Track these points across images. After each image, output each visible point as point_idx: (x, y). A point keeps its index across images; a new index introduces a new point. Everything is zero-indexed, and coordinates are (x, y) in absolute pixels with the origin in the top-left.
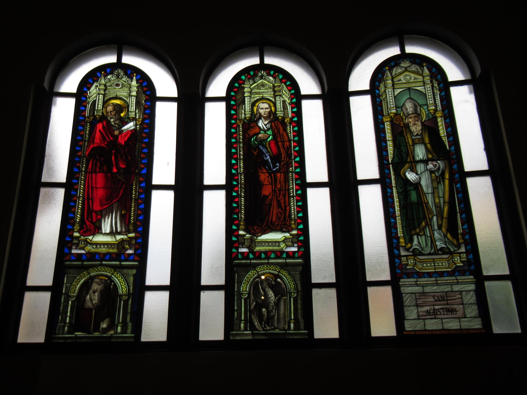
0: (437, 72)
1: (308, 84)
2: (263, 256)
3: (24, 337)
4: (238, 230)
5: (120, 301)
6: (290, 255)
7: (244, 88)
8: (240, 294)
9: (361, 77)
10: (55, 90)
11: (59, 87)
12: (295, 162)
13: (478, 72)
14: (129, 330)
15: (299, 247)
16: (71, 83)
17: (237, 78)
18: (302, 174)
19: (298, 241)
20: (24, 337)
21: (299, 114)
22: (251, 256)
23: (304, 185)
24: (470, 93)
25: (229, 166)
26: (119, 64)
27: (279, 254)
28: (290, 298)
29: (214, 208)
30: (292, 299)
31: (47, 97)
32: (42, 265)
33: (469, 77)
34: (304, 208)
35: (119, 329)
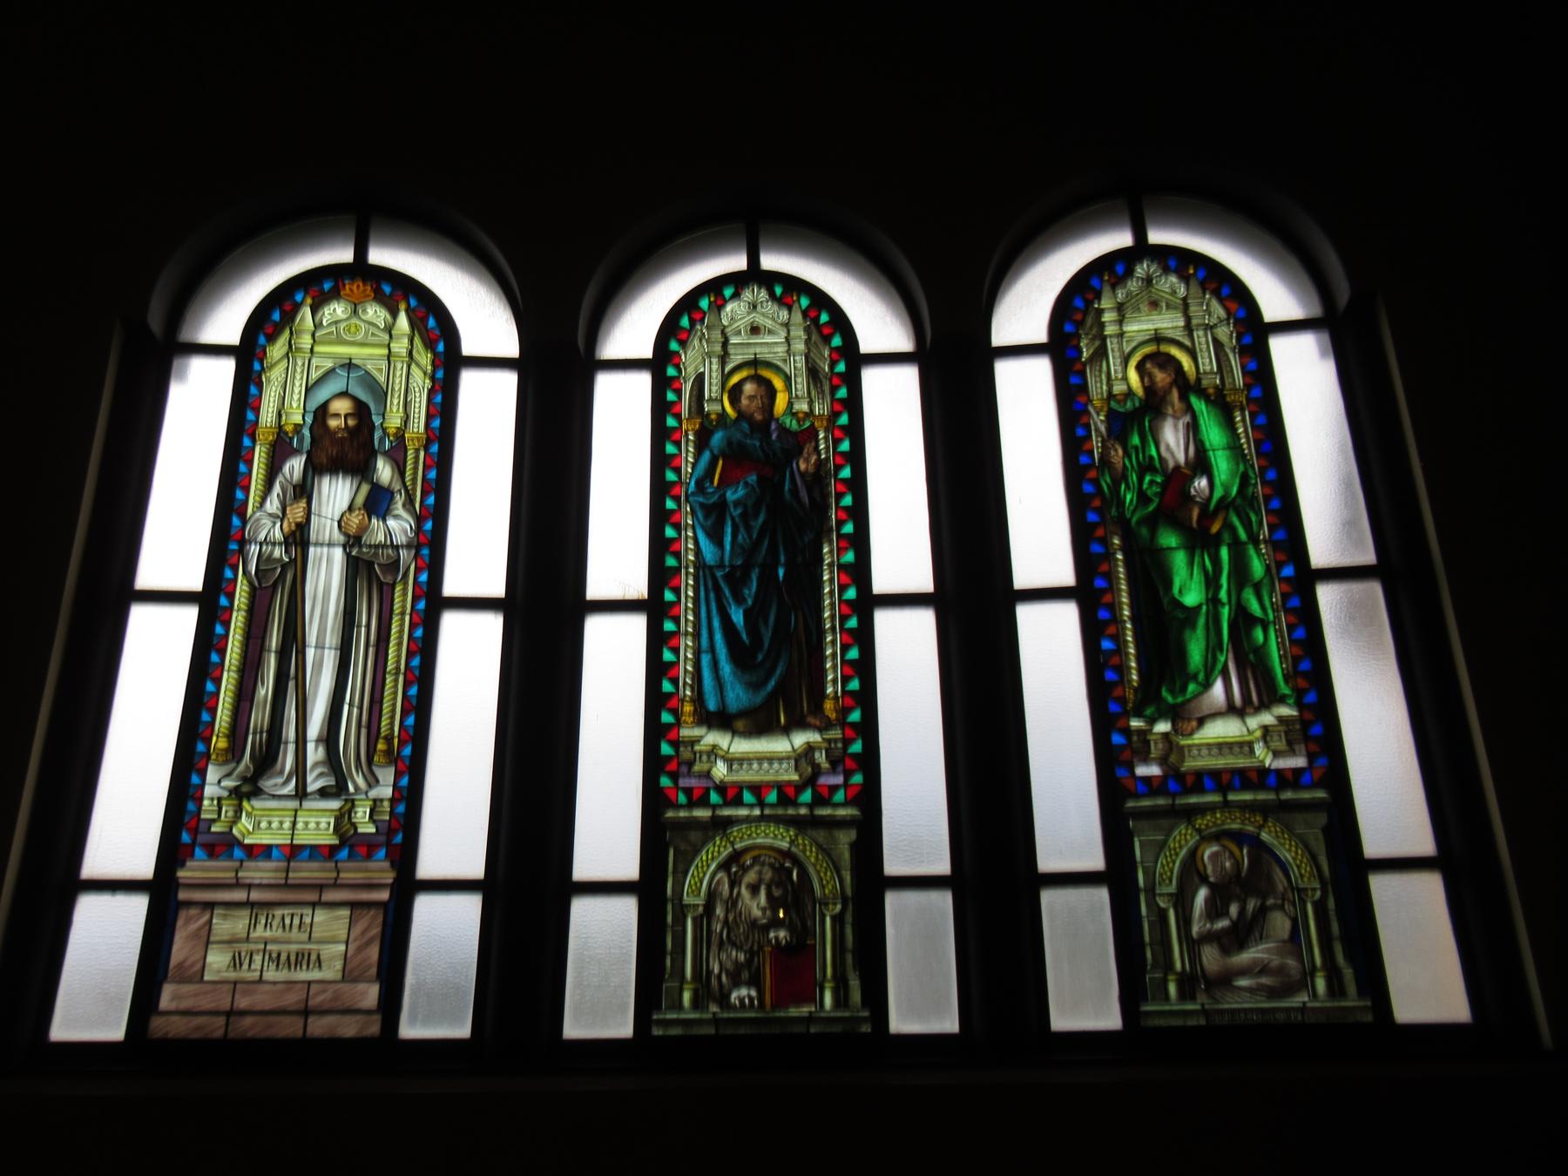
0: (828, 320)
1: (877, 323)
2: (748, 797)
3: (64, 1028)
4: (678, 723)
5: (680, 920)
6: (1290, 779)
7: (1100, 312)
8: (682, 911)
9: (1024, 309)
10: (186, 336)
11: (199, 324)
12: (839, 536)
13: (1343, 294)
14: (1352, 989)
15: (1311, 757)
16: (226, 320)
17: (687, 304)
18: (860, 571)
19: (1307, 739)
20: (64, 1028)
21: (854, 405)
22: (1172, 785)
23: (654, 607)
24: (1323, 354)
25: (659, 547)
26: (360, 269)
27: (1258, 778)
28: (1303, 903)
29: (1050, 647)
30: (828, 920)
31: (165, 351)
32: (125, 821)
33: (1316, 311)
34: (865, 668)
35: (1321, 984)
